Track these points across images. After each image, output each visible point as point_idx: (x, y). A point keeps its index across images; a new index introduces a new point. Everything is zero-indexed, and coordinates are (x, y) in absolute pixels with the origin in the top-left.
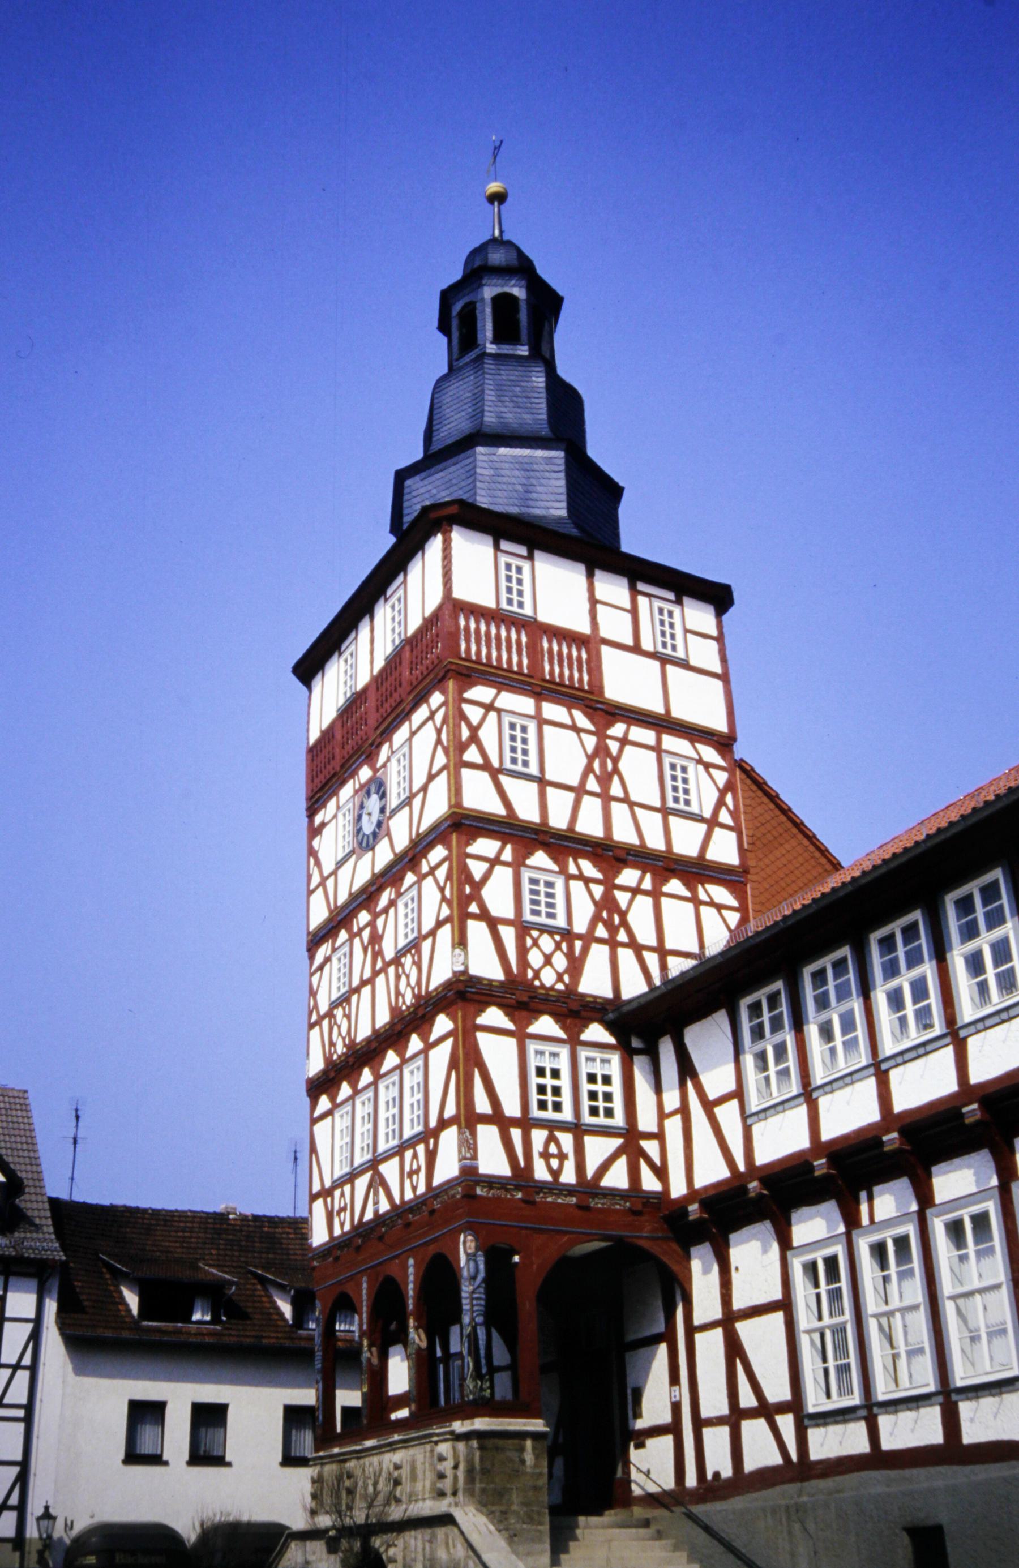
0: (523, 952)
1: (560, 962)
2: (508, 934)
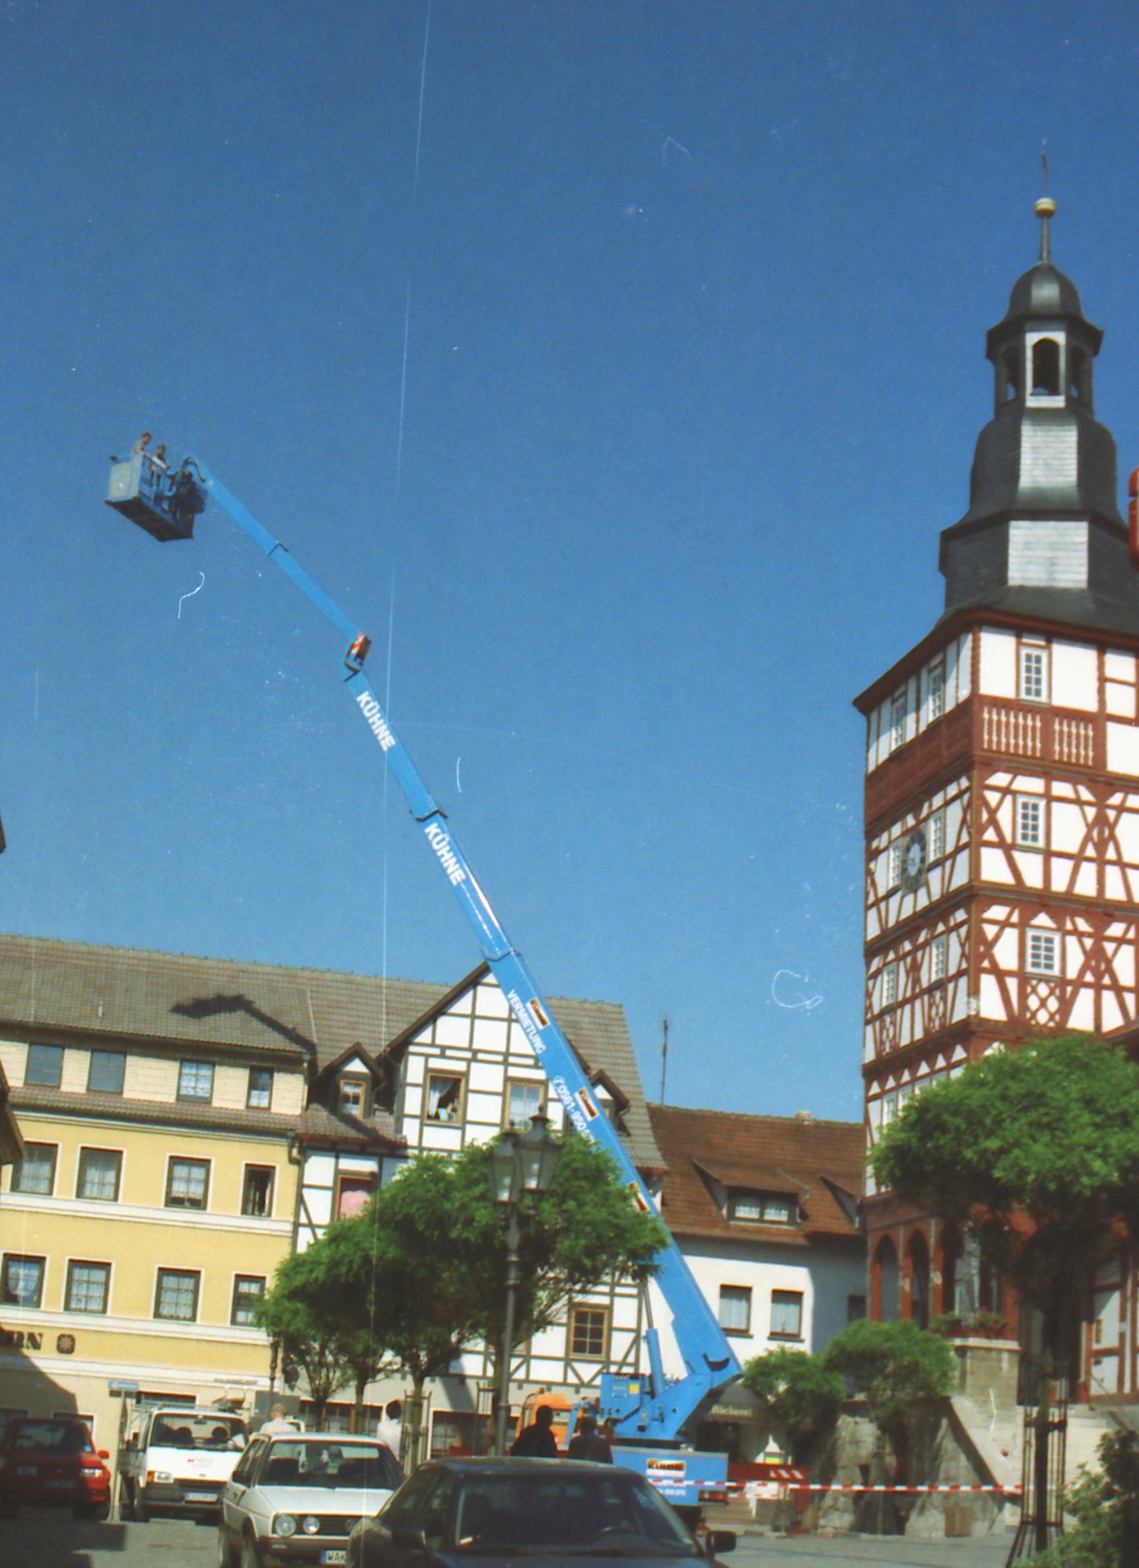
0: (1023, 997)
1: (1053, 1004)
2: (1012, 984)
